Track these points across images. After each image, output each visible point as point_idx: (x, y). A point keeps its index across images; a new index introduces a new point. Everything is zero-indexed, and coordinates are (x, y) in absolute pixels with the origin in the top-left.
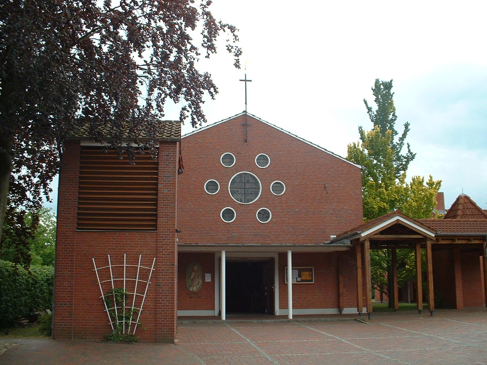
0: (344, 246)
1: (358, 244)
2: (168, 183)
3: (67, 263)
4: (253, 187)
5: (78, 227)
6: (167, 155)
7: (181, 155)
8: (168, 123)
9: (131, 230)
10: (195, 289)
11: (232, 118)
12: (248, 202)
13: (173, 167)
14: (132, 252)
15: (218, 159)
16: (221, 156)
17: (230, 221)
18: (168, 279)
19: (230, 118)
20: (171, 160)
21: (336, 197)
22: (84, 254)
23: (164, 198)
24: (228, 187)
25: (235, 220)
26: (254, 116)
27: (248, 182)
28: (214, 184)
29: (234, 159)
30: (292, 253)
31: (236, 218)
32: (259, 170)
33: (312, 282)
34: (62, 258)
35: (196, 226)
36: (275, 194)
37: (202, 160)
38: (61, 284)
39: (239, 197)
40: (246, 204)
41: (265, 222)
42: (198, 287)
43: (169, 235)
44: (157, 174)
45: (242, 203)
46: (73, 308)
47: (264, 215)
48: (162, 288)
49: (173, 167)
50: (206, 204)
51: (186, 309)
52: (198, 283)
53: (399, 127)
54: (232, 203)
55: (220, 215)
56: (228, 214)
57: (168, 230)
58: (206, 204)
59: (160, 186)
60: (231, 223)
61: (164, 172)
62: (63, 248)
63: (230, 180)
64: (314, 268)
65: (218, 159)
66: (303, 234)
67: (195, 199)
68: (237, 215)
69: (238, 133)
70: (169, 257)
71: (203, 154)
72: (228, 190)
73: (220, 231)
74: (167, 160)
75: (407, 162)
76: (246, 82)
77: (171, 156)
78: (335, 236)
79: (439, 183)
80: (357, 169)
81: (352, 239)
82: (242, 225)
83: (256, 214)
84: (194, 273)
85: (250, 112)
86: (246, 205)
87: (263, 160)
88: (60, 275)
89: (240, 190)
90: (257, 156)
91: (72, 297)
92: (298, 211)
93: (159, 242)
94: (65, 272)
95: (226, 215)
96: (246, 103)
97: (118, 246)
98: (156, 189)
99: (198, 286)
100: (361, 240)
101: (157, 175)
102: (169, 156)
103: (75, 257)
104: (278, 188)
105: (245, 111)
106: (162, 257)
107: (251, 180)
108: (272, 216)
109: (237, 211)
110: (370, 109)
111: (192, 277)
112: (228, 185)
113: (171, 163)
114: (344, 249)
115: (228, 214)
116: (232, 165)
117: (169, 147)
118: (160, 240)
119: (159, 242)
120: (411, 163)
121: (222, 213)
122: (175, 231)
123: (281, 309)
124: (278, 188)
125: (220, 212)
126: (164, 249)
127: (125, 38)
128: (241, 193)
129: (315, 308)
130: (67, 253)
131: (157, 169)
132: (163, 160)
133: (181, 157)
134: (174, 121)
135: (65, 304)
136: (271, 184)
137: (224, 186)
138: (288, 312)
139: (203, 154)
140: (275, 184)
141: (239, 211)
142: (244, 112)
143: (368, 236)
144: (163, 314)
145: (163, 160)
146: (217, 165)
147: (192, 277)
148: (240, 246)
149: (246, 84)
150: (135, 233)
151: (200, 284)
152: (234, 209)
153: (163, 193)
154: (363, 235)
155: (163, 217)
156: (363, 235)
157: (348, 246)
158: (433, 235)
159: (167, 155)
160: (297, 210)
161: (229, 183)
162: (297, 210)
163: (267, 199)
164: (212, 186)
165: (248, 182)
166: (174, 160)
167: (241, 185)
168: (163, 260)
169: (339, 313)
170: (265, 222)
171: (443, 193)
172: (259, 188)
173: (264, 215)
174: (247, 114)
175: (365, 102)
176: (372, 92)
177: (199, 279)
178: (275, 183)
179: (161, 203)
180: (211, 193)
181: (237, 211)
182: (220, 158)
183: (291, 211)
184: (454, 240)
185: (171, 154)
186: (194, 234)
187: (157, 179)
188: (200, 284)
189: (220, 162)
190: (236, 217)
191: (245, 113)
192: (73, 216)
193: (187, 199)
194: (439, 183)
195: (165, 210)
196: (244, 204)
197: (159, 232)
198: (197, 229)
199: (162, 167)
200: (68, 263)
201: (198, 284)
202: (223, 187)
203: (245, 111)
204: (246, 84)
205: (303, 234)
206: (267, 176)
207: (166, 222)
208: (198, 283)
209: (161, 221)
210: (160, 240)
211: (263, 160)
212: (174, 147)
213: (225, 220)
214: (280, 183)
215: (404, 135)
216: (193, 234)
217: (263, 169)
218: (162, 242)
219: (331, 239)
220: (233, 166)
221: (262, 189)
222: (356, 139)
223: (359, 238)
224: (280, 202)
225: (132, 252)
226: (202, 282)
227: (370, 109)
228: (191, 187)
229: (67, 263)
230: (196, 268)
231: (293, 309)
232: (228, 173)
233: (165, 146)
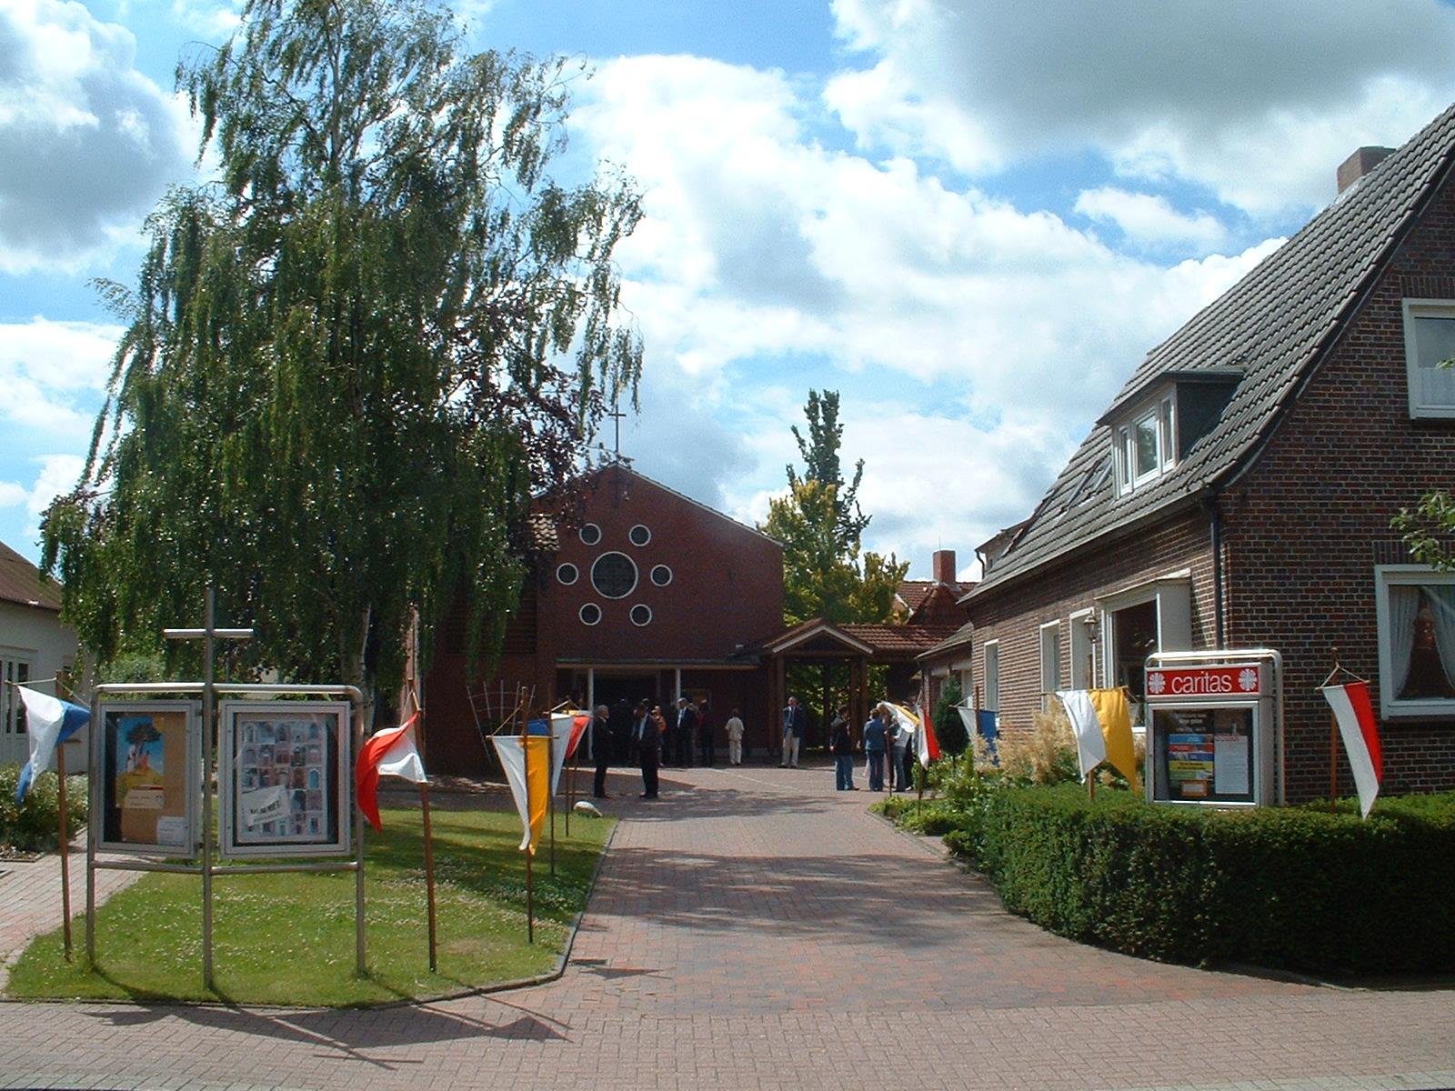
1: (768, 659)
53: (846, 471)
75: (859, 530)
76: (617, 420)
79: (905, 567)
87: (640, 535)
110: (802, 442)
116: (637, 574)
120: (863, 530)
124: (660, 576)
127: (250, 185)
137: (585, 573)
158: (871, 652)
163: (645, 592)
171: (953, 553)
173: (641, 615)
175: (794, 430)
176: (805, 415)
184: (905, 657)
194: (905, 567)
206: (646, 558)
211: (640, 535)
215: (857, 480)
222: (784, 493)
227: (802, 442)
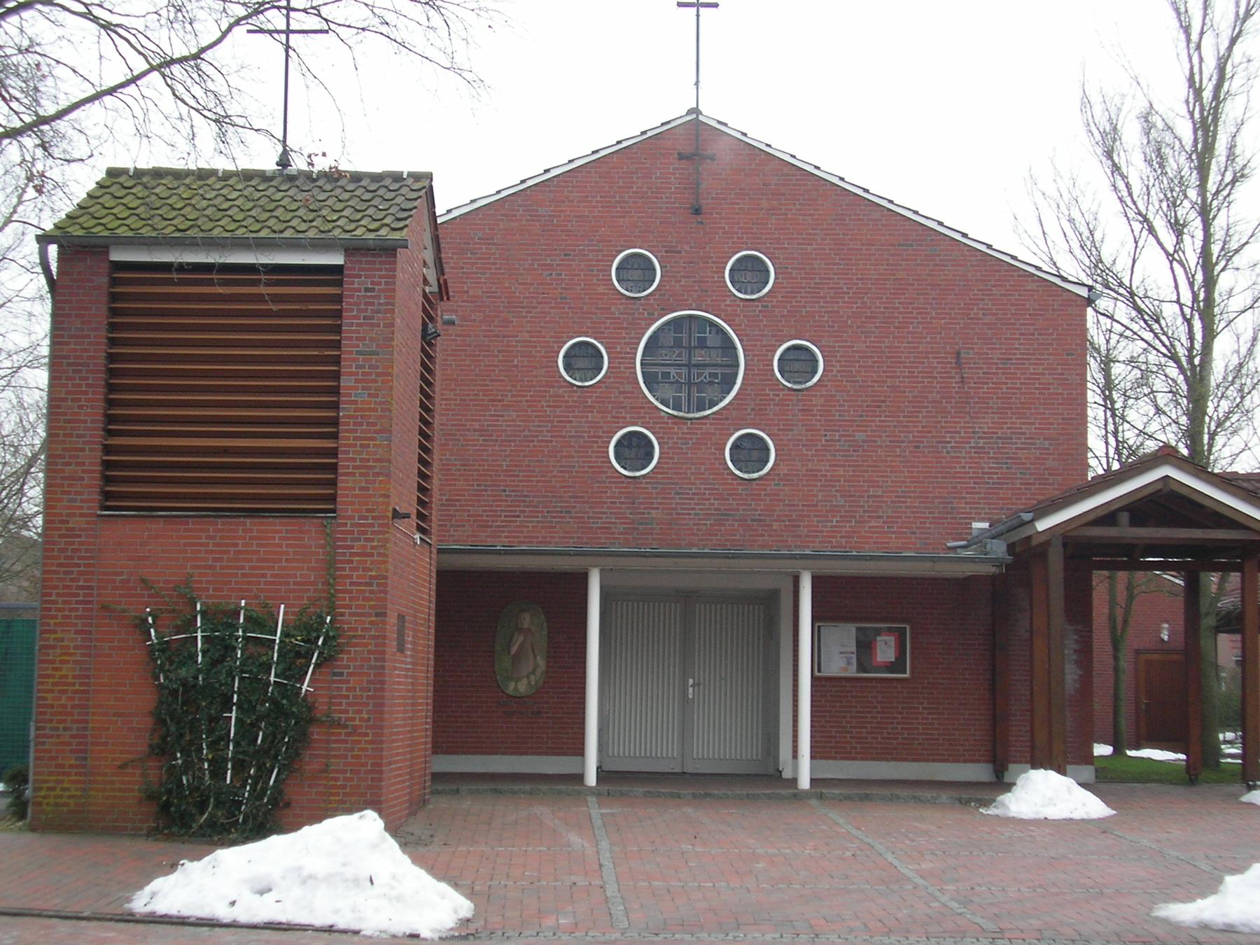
0: (982, 561)
2: (370, 374)
3: (71, 610)
4: (719, 360)
5: (108, 504)
6: (367, 290)
7: (443, 274)
8: (387, 182)
9: (304, 511)
10: (522, 687)
11: (649, 134)
12: (700, 409)
13: (386, 326)
14: (264, 576)
15: (602, 270)
16: (613, 262)
17: (638, 470)
18: (366, 655)
19: (523, 182)
20: (380, 304)
21: (994, 393)
22: (122, 581)
23: (357, 417)
24: (635, 363)
25: (655, 467)
26: (726, 125)
27: (702, 343)
28: (590, 351)
29: (654, 270)
30: (813, 577)
31: (658, 463)
32: (739, 306)
33: (905, 673)
34: (58, 595)
35: (528, 486)
36: (789, 385)
37: (551, 275)
38: (55, 669)
39: (670, 393)
40: (691, 415)
41: (755, 475)
42: (533, 683)
43: (372, 525)
44: (337, 345)
45: (681, 414)
46: (90, 740)
47: (750, 452)
48: (348, 682)
49: (386, 326)
50: (564, 416)
51: (492, 751)
52: (534, 670)
54: (644, 412)
55: (608, 452)
56: (635, 449)
57: (367, 510)
58: (564, 416)
59: (345, 382)
60: (644, 476)
61: (357, 339)
62: (60, 565)
63: (640, 339)
64: (912, 629)
65: (602, 270)
66: (879, 517)
67: (527, 401)
68: (661, 453)
69: (670, 183)
70: (371, 592)
71: (556, 255)
72: (635, 373)
73: (606, 503)
74: (367, 304)
77: (380, 290)
78: (985, 525)
80: (1073, 301)
81: (1012, 540)
82: (677, 484)
83: (724, 450)
84: (521, 639)
85: (712, 111)
86: (691, 419)
87: (750, 271)
88: (52, 643)
89: (673, 371)
90: (731, 257)
91: (86, 707)
92: (863, 441)
93: (340, 547)
94: (66, 636)
95: (626, 452)
96: (697, 83)
97: (221, 560)
98: (336, 391)
99: (532, 677)
100: (1034, 542)
101: (339, 348)
102: (373, 290)
103: (95, 592)
104: (799, 362)
105: (695, 111)
106: (351, 592)
107: (713, 340)
108: (776, 456)
109: (663, 438)
111: (514, 649)
112: (635, 354)
113: (378, 312)
114: (990, 569)
115: (635, 449)
117: (374, 263)
118: (345, 540)
119: (340, 547)
121: (615, 447)
122: (390, 515)
123: (822, 758)
124: (799, 362)
125: (609, 442)
126: (356, 569)
128: (677, 382)
129: (842, 758)
130: (72, 580)
131: (338, 329)
132: (355, 304)
133: (445, 281)
134: (410, 175)
135: (65, 729)
136: (775, 351)
137: (622, 359)
138: (583, 764)
139: (556, 255)
140: (791, 352)
141: (669, 438)
142: (690, 112)
143: (1063, 526)
144: (349, 760)
145: (355, 304)
146: (601, 289)
147: (514, 649)
148: (644, 555)
149: (698, 16)
150: (271, 520)
151: (539, 671)
152: (653, 433)
153: (355, 402)
154: (1042, 525)
155: (353, 474)
156: (1042, 525)
157: (996, 562)
159: (367, 290)
160: (860, 436)
161: (637, 349)
162: (860, 436)
164: (584, 358)
165: (702, 343)
166: (388, 304)
167: (680, 355)
168: (351, 599)
169: (993, 779)
170: (755, 475)
172: (738, 366)
173: (750, 452)
174: (701, 118)
177: (535, 657)
178: (789, 349)
179: (347, 431)
180: (581, 380)
181: (663, 438)
182: (611, 266)
183: (839, 441)
185: (380, 283)
186: (525, 511)
187: (337, 360)
188: (539, 671)
189: (611, 280)
190: (660, 458)
191: (694, 116)
192: (621, 338)
193: (503, 400)
195: (361, 453)
196: (686, 415)
197: (344, 518)
198: (534, 496)
199: (352, 325)
200: (76, 610)
201: (533, 672)
202: (620, 363)
203: (695, 111)
204: (698, 16)
205: (879, 517)
207: (361, 488)
208: (534, 670)
209: (348, 485)
210: (345, 540)
211: (750, 271)
212: (389, 263)
213: (625, 469)
214: (806, 349)
216: (521, 511)
217: (752, 303)
218: (352, 547)
219: (975, 533)
220: (650, 294)
221: (745, 369)
223: (1029, 538)
224: (804, 410)
225: (264, 576)
226: (548, 667)
228: (516, 363)
229: (71, 610)
230: (526, 620)
231: (812, 758)
232: (638, 315)
233: (361, 262)
